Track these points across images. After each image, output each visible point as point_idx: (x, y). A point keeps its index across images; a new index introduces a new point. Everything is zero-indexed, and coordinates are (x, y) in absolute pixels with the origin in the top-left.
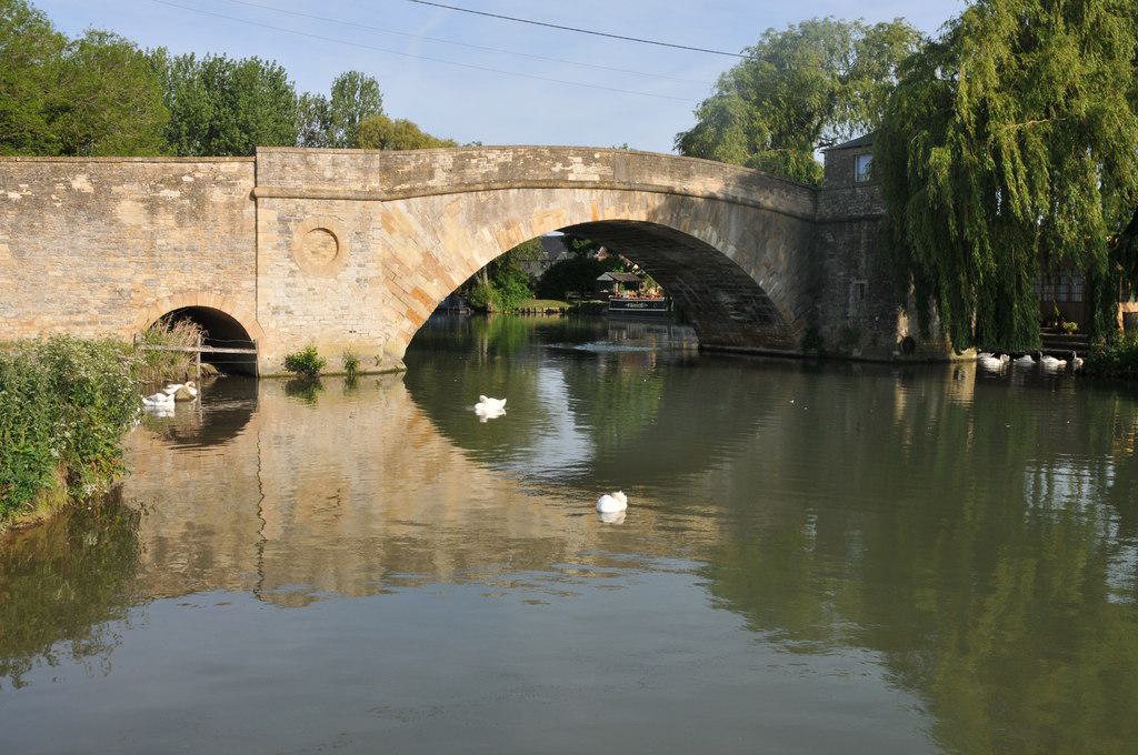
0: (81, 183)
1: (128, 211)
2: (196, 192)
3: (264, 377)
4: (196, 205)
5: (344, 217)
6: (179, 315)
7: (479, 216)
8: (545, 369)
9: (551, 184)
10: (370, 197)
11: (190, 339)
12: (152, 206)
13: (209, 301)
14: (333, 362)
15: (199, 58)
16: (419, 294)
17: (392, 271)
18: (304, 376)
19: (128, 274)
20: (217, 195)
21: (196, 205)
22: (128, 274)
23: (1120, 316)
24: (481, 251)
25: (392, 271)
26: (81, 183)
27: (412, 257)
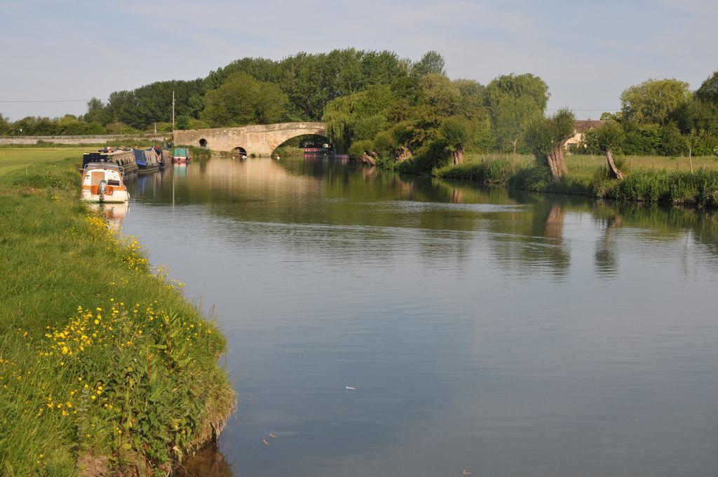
0: (225, 131)
1: (230, 134)
2: (239, 132)
3: (266, 157)
4: (239, 134)
5: (260, 134)
6: (237, 148)
7: (283, 134)
8: (199, 165)
9: (296, 129)
10: (263, 132)
11: (238, 151)
12: (233, 134)
13: (240, 146)
14: (257, 155)
15: (36, 117)
16: (273, 146)
17: (268, 142)
18: (253, 156)
19: (230, 143)
20: (242, 132)
21: (239, 134)
22: (230, 143)
23: (365, 175)
24: (284, 139)
25: (268, 142)
26: (225, 131)
27: (272, 140)
